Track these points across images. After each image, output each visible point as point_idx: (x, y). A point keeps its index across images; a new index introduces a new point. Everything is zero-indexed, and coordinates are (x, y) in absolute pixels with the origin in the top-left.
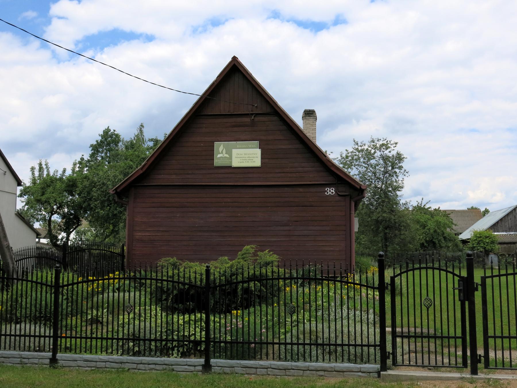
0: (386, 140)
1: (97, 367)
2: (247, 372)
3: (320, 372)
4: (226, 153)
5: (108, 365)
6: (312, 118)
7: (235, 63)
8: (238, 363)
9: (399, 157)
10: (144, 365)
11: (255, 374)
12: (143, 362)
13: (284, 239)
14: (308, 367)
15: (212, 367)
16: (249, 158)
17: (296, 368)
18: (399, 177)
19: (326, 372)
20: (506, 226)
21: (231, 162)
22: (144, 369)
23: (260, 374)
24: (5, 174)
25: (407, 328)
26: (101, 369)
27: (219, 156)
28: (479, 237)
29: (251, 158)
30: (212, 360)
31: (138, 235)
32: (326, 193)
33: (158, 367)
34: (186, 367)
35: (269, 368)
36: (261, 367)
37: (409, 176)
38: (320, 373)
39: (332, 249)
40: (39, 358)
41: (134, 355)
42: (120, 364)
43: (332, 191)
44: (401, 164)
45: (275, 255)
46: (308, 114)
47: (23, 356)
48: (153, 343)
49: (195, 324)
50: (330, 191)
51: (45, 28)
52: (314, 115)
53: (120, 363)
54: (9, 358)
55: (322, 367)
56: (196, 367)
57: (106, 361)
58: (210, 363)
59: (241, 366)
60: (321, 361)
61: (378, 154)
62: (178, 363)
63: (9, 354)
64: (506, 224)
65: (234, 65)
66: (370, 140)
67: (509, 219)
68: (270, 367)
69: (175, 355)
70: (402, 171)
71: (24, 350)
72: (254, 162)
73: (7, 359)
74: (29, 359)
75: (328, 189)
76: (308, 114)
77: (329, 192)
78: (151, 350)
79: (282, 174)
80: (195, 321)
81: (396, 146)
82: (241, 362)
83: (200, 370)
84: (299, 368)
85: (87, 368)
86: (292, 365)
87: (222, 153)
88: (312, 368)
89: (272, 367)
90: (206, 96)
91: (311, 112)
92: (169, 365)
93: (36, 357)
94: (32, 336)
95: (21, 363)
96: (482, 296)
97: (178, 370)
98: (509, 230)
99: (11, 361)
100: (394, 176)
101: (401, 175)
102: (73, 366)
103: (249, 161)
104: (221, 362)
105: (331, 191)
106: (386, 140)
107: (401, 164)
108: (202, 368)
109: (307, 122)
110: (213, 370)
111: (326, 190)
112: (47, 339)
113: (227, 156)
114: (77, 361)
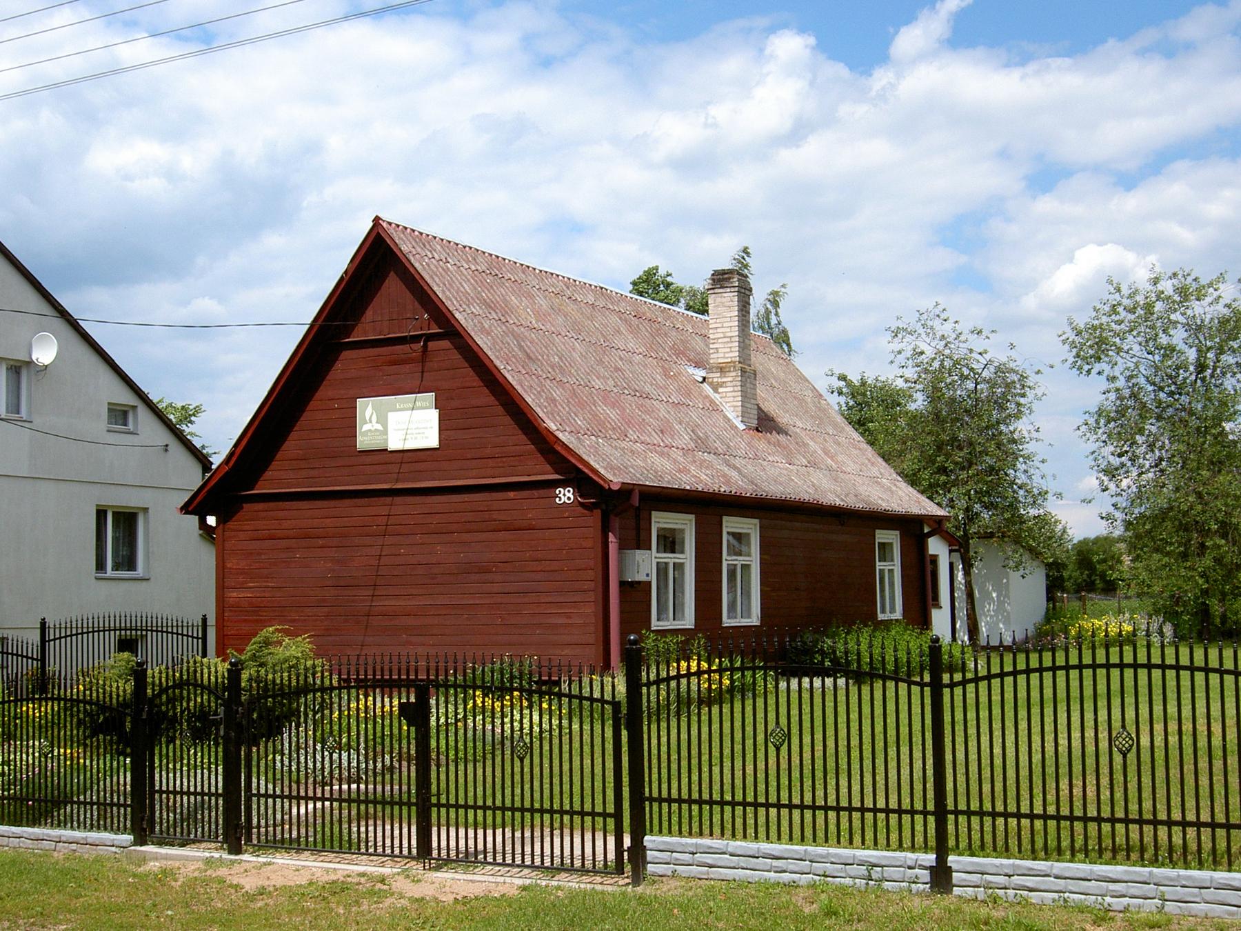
4: (377, 422)
6: (728, 290)
16: (417, 431)
21: (386, 440)
24: (166, 450)
27: (366, 428)
29: (421, 431)
30: (951, 858)
31: (233, 595)
43: (568, 495)
46: (719, 280)
50: (564, 495)
58: (642, 843)
60: (847, 844)
72: (427, 438)
75: (560, 491)
76: (719, 280)
77: (563, 497)
87: (371, 422)
94: (808, 807)
103: (418, 436)
105: (566, 495)
109: (719, 300)
112: (919, 819)
113: (379, 427)
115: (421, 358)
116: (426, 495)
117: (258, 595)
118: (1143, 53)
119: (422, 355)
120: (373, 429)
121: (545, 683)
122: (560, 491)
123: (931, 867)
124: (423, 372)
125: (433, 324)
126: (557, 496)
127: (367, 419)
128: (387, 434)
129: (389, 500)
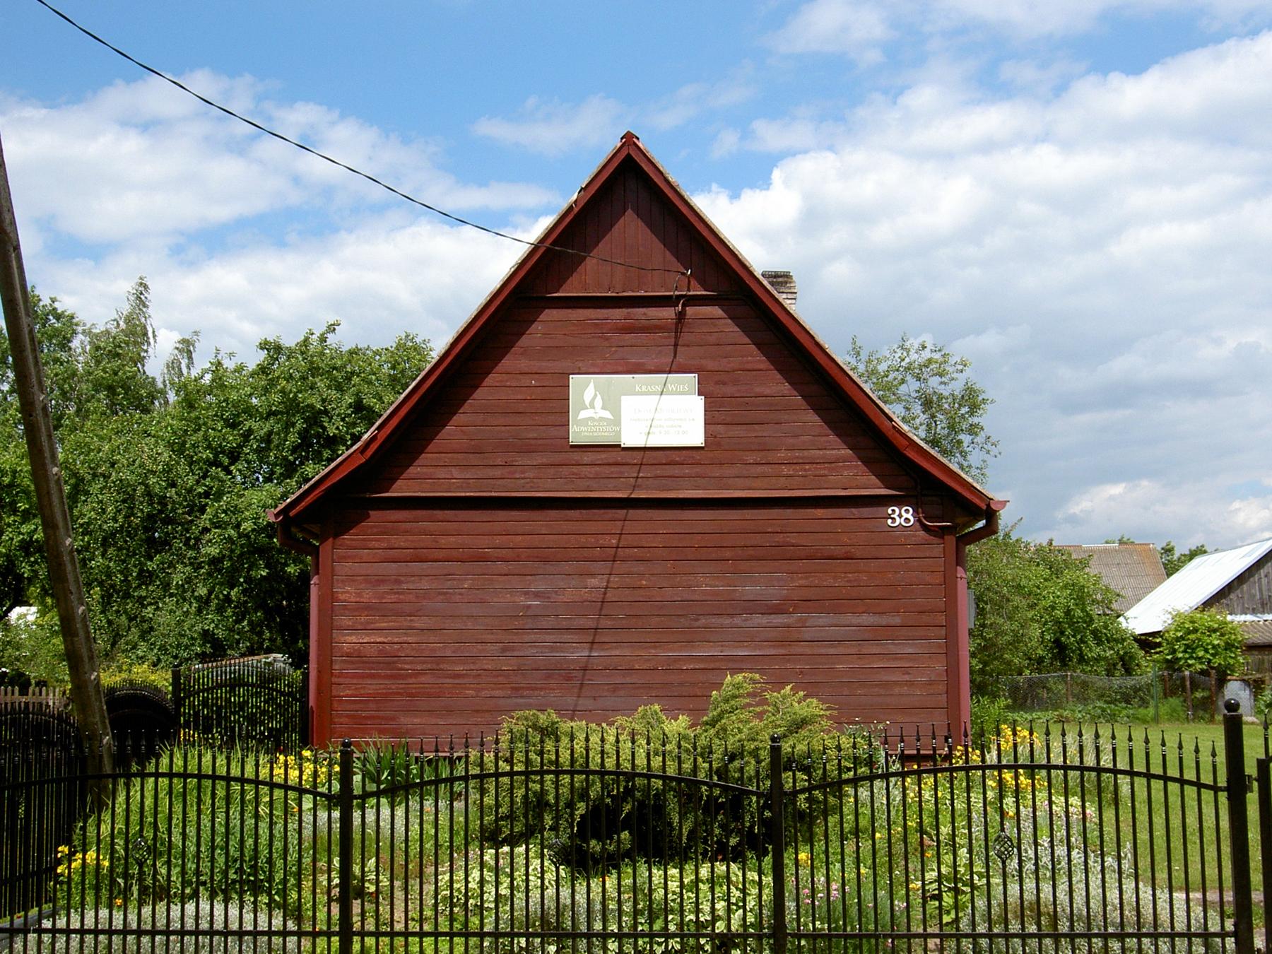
0: (940, 351)
7: (631, 152)
9: (971, 399)
13: (773, 652)
20: (1255, 596)
25: (1218, 891)
27: (583, 415)
28: (1189, 632)
32: (889, 521)
37: (999, 456)
43: (905, 515)
44: (975, 420)
50: (900, 516)
51: (714, 187)
52: (790, 288)
64: (1253, 591)
65: (629, 158)
67: (1263, 575)
70: (980, 439)
72: (684, 432)
75: (893, 511)
77: (898, 519)
79: (767, 469)
80: (712, 881)
90: (547, 244)
96: (1245, 802)
98: (1263, 608)
101: (977, 450)
105: (903, 516)
106: (940, 351)
107: (975, 420)
111: (890, 512)
113: (607, 414)
122: (893, 511)
127: (587, 403)
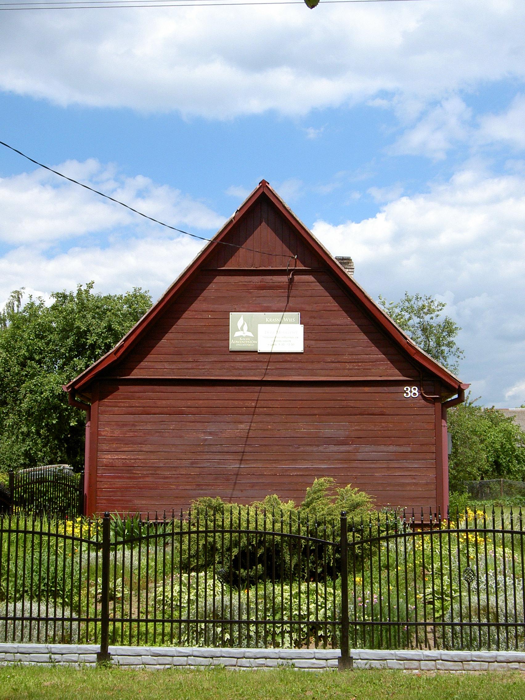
0: (429, 299)
1: (175, 664)
2: (406, 667)
3: (513, 663)
4: (248, 331)
5: (191, 660)
8: (392, 654)
10: (248, 660)
11: (417, 669)
12: (247, 655)
14: (496, 658)
15: (354, 661)
17: (479, 660)
18: (448, 359)
19: (521, 664)
22: (248, 665)
23: (426, 668)
26: (181, 667)
27: (237, 334)
32: (405, 395)
33: (269, 662)
34: (314, 661)
35: (439, 660)
36: (427, 659)
38: (513, 665)
39: (414, 481)
40: (80, 652)
41: (224, 645)
42: (211, 659)
43: (413, 391)
44: (451, 339)
45: (364, 493)
47: (53, 650)
48: (253, 628)
49: (308, 597)
50: (411, 392)
52: (350, 266)
53: (210, 658)
54: (29, 654)
55: (516, 657)
56: (328, 661)
57: (187, 654)
59: (397, 658)
61: (415, 320)
62: (301, 656)
63: (31, 648)
66: (404, 298)
68: (439, 658)
69: (287, 644)
71: (54, 642)
73: (27, 655)
74: (62, 654)
75: (407, 389)
77: (409, 393)
78: (249, 637)
79: (338, 365)
81: (441, 310)
82: (397, 653)
83: (335, 665)
84: (482, 660)
85: (158, 666)
86: (472, 655)
88: (502, 659)
89: (443, 658)
91: (345, 261)
92: (288, 659)
93: (75, 651)
95: (51, 660)
97: (300, 666)
99: (31, 658)
100: (441, 358)
102: (135, 663)
104: (366, 653)
105: (412, 392)
106: (429, 299)
107: (451, 339)
108: (338, 662)
110: (355, 665)
111: (405, 389)
113: (250, 334)
114: (141, 656)
115: (287, 286)
116: (291, 386)
117: (132, 457)
118: (43, 184)
119: (289, 286)
120: (244, 335)
121: (418, 526)
122: (407, 389)
123: (339, 657)
124: (288, 297)
125: (298, 262)
126: (405, 392)
127: (239, 328)
128: (257, 340)
129: (257, 388)
